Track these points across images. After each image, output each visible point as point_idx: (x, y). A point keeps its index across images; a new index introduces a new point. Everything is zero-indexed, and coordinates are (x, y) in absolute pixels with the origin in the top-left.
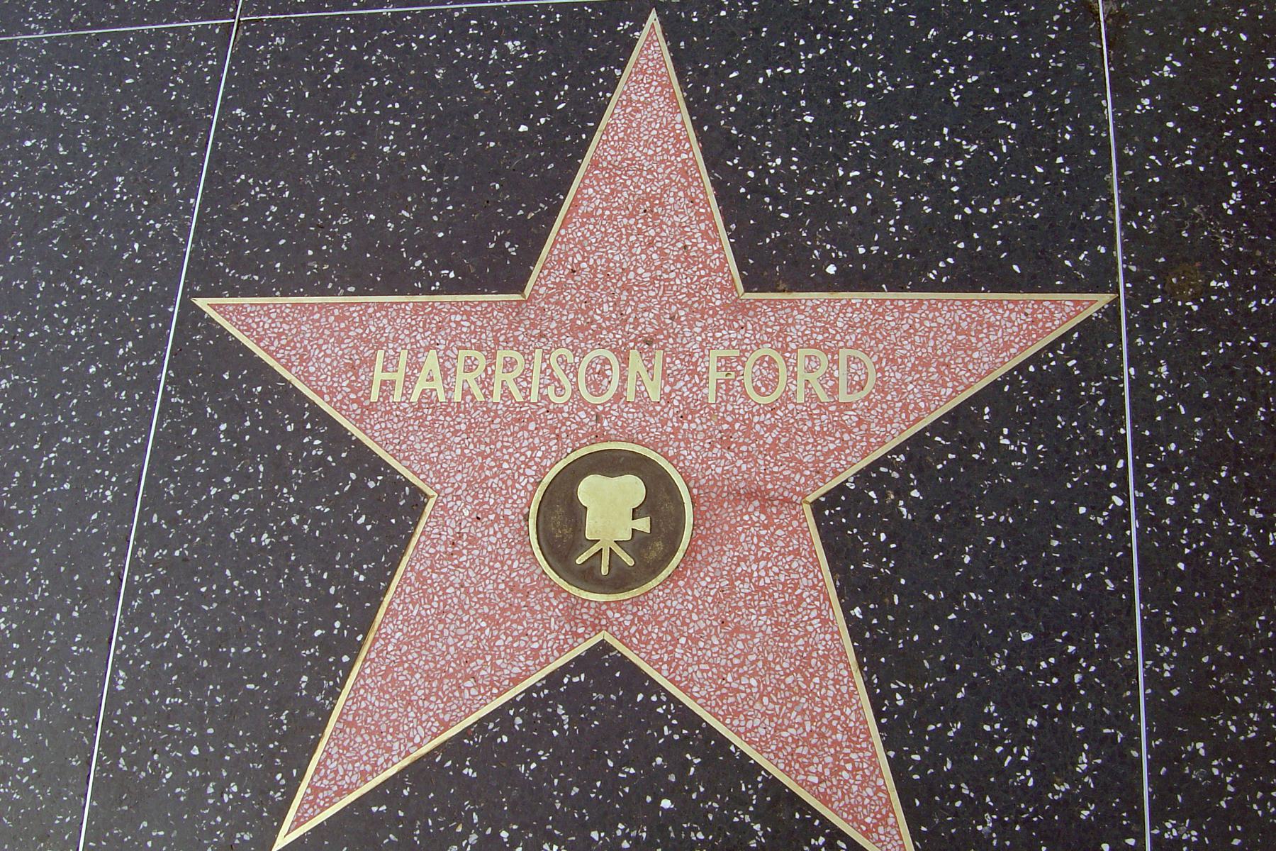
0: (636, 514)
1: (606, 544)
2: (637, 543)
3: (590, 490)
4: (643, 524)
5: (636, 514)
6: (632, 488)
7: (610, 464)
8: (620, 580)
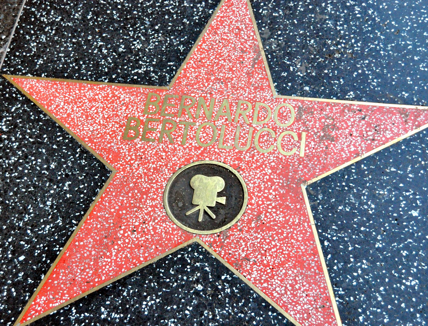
0: (220, 194)
2: (217, 208)
3: (198, 181)
4: (223, 200)
5: (220, 194)
6: (218, 183)
7: (212, 170)
8: (210, 224)
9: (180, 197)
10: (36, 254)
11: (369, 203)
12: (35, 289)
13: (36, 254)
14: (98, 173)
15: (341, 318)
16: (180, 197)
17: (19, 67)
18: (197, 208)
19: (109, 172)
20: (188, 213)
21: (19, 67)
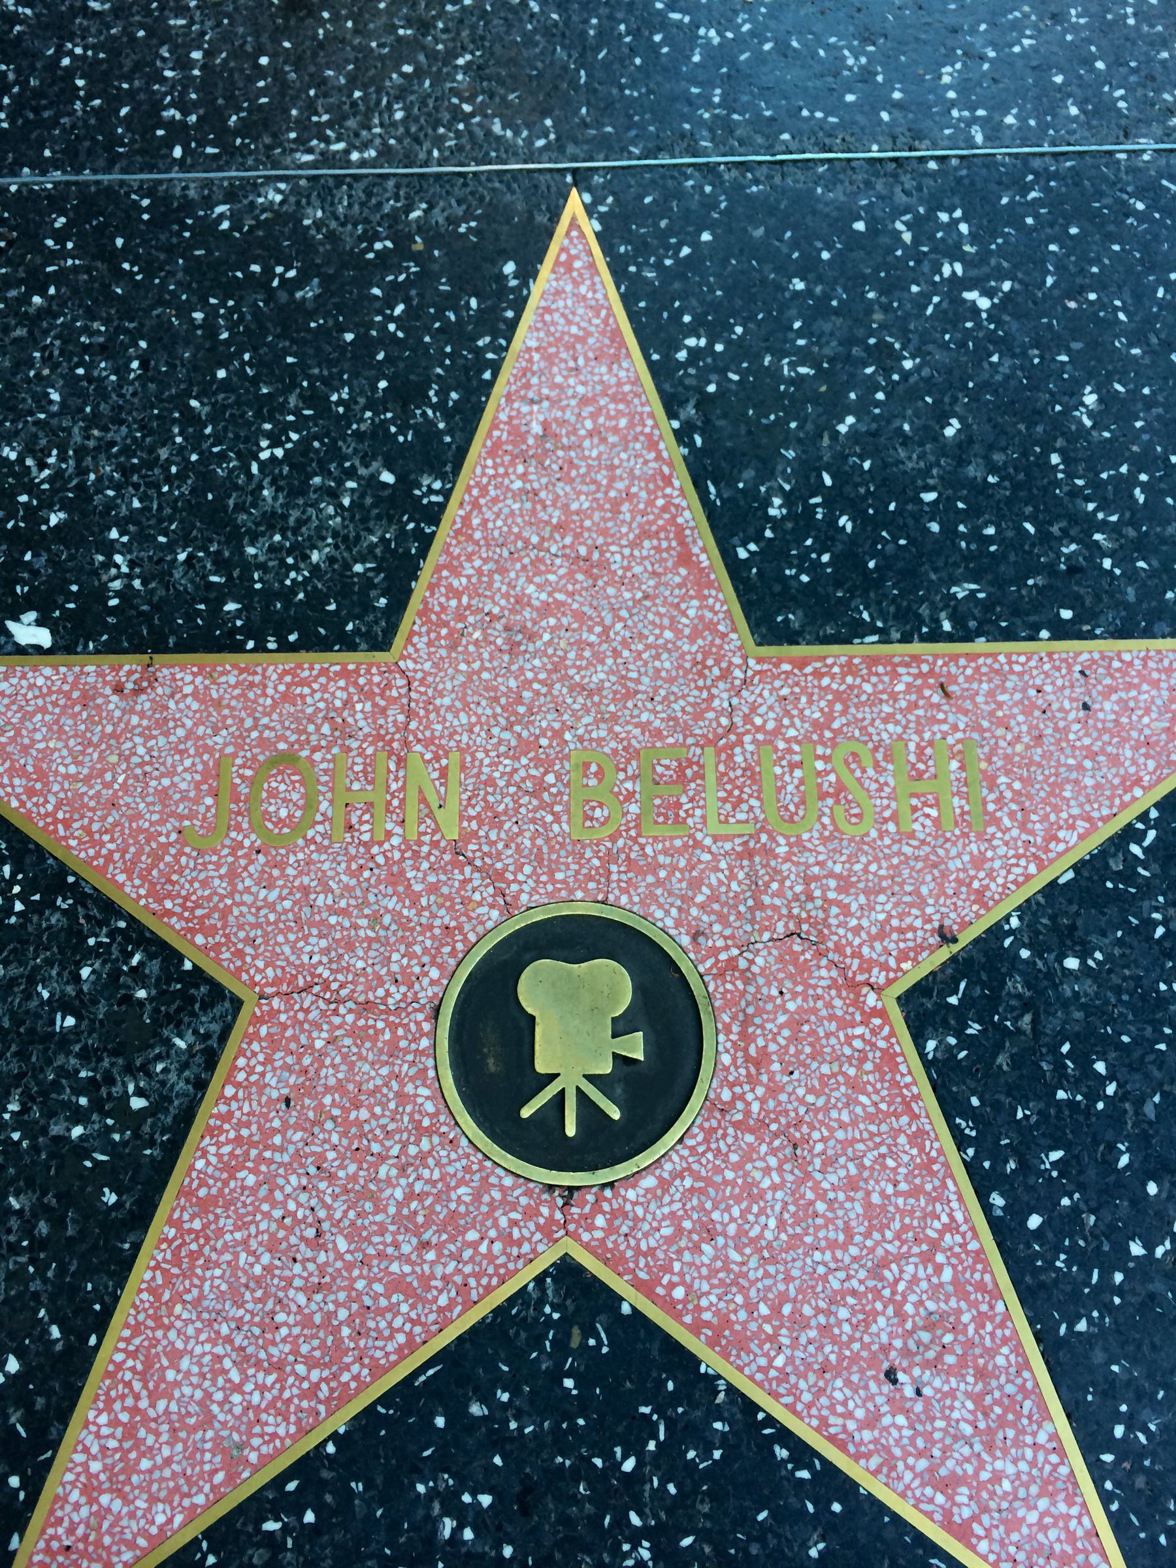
0: (621, 1027)
1: (570, 1082)
3: (538, 987)
4: (635, 1047)
5: (621, 1027)
6: (613, 983)
8: (604, 1145)
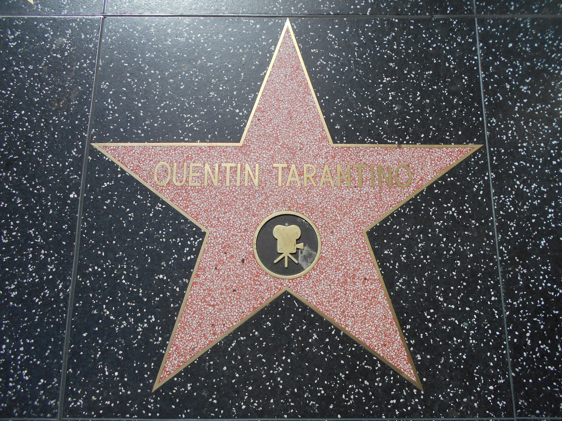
0: (298, 241)
3: (278, 231)
6: (295, 231)
9: (266, 245)
10: (185, 251)
11: (164, 233)
12: (168, 342)
13: (185, 251)
14: (368, 233)
15: (246, 322)
16: (266, 245)
17: (25, 357)
18: (286, 259)
19: (204, 233)
20: (286, 266)
21: (25, 357)
